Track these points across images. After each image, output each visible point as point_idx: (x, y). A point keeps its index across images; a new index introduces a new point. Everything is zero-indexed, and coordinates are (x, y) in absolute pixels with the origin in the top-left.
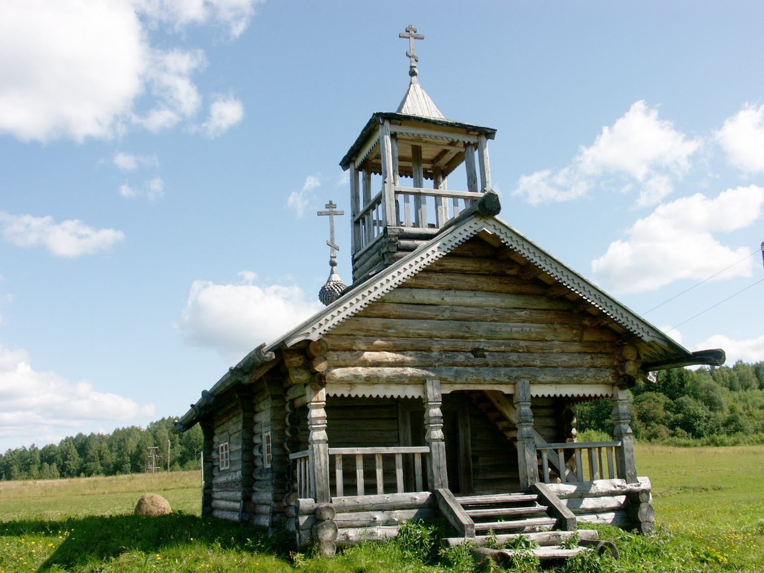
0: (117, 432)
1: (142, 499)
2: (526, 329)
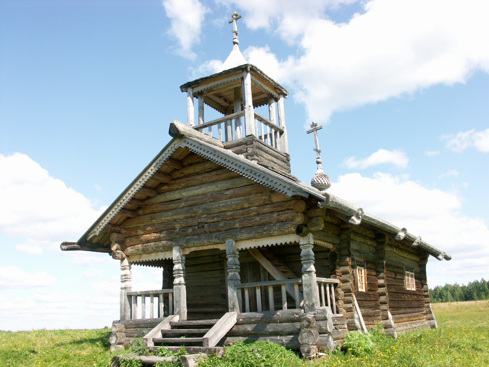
2: (228, 203)
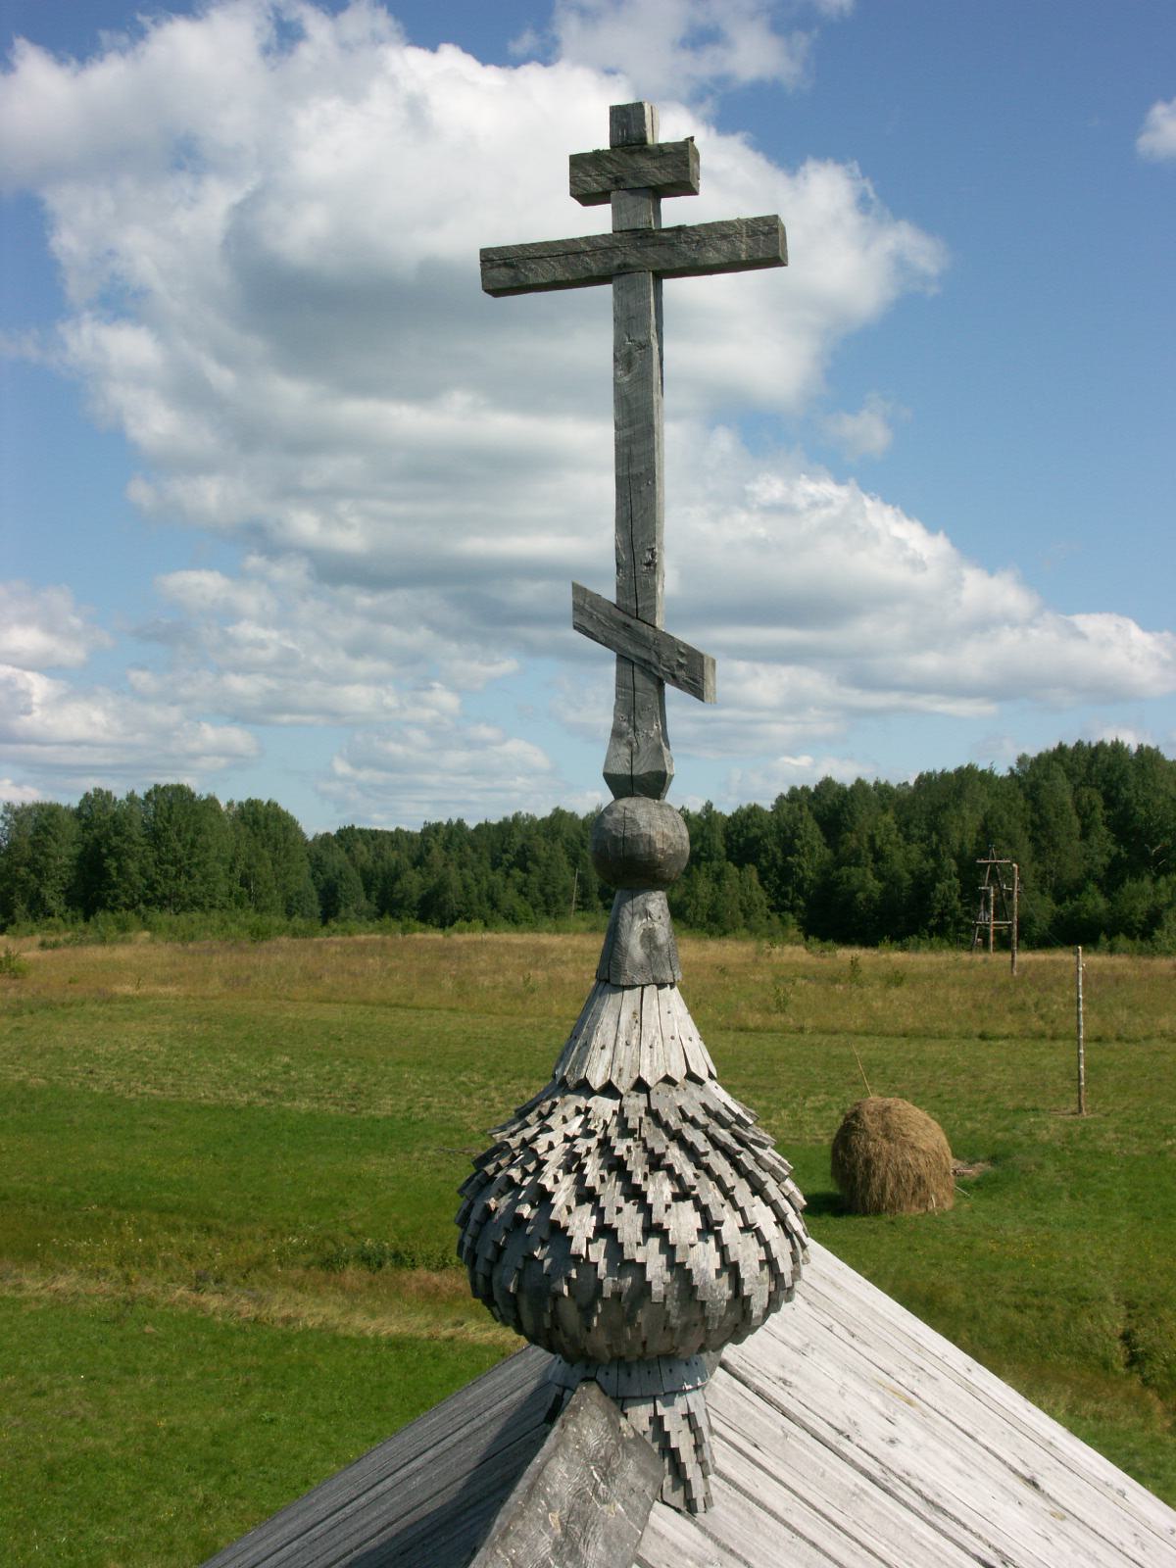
0: (925, 781)
1: (856, 1115)
